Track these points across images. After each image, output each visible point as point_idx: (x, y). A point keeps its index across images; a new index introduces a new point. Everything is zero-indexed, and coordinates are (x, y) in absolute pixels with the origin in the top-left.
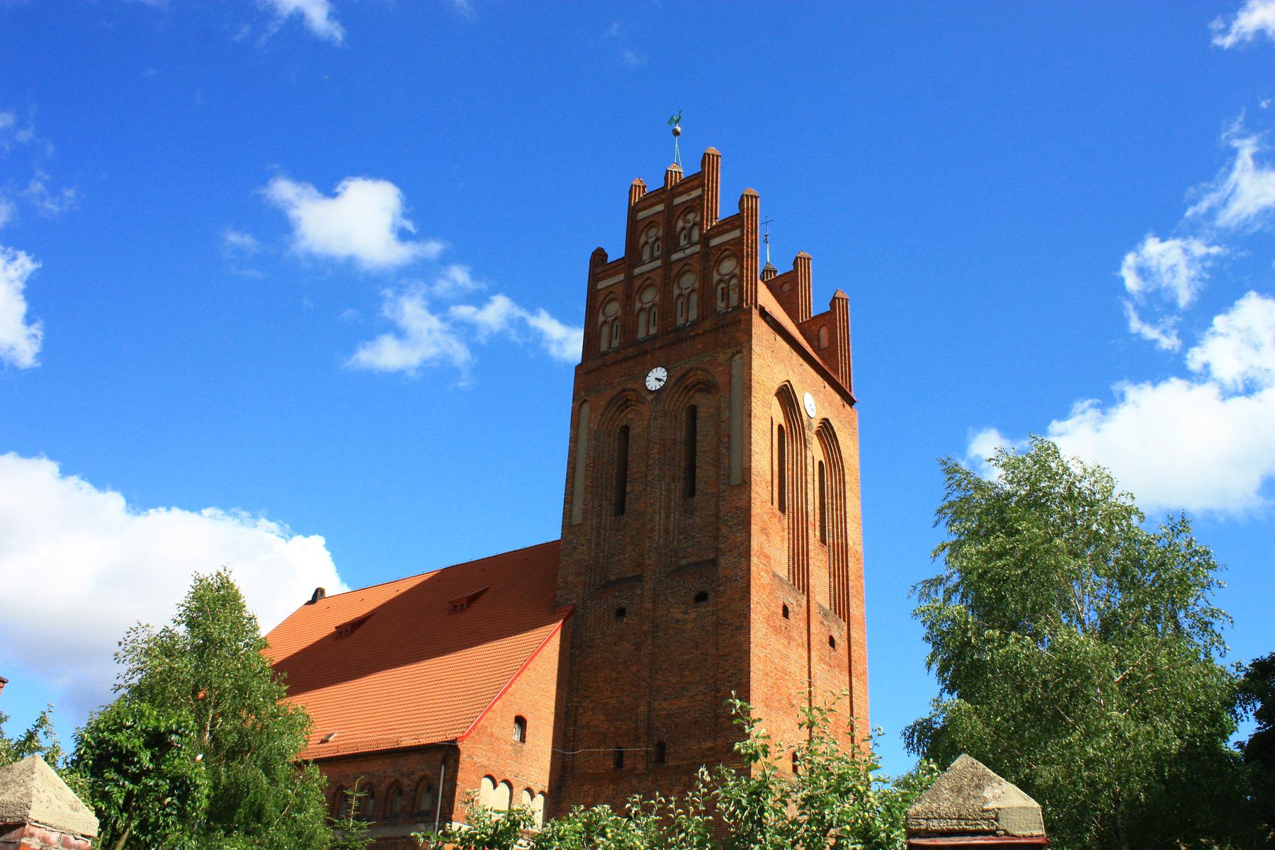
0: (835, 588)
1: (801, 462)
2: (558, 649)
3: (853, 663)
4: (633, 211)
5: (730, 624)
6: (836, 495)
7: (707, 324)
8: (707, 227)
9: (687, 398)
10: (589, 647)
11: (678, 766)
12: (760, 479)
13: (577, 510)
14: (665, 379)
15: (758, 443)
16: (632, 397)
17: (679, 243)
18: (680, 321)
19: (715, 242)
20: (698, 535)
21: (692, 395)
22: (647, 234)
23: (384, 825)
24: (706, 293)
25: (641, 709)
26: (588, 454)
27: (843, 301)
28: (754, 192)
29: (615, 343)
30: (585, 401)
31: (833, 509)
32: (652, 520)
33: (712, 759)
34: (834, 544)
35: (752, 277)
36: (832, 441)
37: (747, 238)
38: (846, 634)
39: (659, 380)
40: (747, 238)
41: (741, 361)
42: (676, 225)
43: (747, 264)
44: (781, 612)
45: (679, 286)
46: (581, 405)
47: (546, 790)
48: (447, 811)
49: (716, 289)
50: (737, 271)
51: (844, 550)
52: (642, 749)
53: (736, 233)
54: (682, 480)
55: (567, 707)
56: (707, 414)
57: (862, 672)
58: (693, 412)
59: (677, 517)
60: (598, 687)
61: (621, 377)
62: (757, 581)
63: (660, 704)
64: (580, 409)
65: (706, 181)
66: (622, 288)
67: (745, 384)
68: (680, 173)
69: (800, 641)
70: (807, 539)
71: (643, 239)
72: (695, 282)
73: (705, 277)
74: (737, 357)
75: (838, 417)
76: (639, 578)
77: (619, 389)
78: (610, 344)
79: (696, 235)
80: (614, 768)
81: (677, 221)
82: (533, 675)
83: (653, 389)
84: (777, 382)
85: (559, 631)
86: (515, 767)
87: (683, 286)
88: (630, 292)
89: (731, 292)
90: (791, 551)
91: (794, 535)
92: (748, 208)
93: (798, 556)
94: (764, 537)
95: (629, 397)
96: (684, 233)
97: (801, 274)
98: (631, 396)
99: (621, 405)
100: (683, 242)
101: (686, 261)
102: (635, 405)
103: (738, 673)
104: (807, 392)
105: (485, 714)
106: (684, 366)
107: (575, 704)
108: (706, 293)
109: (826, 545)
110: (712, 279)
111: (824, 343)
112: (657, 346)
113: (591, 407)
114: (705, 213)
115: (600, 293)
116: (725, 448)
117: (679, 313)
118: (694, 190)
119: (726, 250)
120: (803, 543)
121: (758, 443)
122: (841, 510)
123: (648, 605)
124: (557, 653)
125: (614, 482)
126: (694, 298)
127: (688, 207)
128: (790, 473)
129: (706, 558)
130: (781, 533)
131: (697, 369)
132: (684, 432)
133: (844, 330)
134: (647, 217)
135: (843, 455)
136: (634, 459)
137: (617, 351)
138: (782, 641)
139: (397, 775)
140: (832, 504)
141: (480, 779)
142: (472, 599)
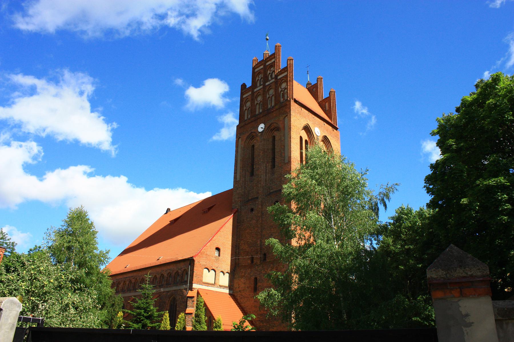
2: (232, 224)
4: (254, 69)
7: (277, 107)
8: (277, 72)
9: (272, 133)
10: (243, 222)
11: (270, 261)
12: (295, 160)
13: (238, 177)
14: (264, 127)
15: (294, 147)
16: (254, 135)
17: (268, 79)
18: (269, 106)
19: (279, 77)
20: (276, 181)
21: (273, 133)
22: (258, 77)
23: (174, 286)
24: (277, 95)
25: (258, 243)
26: (241, 156)
27: (333, 92)
28: (291, 58)
30: (240, 138)
32: (261, 177)
35: (291, 88)
36: (329, 143)
37: (289, 75)
39: (262, 128)
40: (289, 75)
43: (289, 84)
45: (269, 94)
46: (239, 139)
47: (229, 272)
49: (280, 94)
50: (286, 87)
52: (259, 256)
53: (285, 74)
54: (271, 163)
55: (236, 243)
58: (274, 138)
61: (251, 128)
64: (238, 141)
65: (276, 56)
66: (251, 97)
67: (289, 127)
68: (268, 53)
71: (257, 79)
73: (276, 90)
75: (331, 134)
76: (257, 198)
77: (250, 132)
78: (248, 117)
79: (273, 76)
80: (251, 263)
82: (222, 233)
83: (260, 131)
84: (302, 125)
85: (232, 218)
86: (216, 265)
87: (270, 94)
88: (253, 98)
92: (289, 64)
95: (253, 135)
96: (270, 75)
97: (319, 84)
98: (254, 134)
99: (251, 138)
100: (270, 78)
102: (256, 137)
104: (316, 127)
105: (203, 247)
106: (270, 122)
107: (238, 242)
108: (277, 95)
110: (279, 91)
111: (327, 108)
113: (242, 139)
114: (276, 67)
115: (244, 99)
116: (283, 150)
117: (269, 104)
119: (283, 80)
121: (294, 147)
123: (260, 207)
124: (232, 225)
125: (250, 165)
126: (273, 98)
127: (271, 66)
131: (274, 123)
132: (271, 146)
133: (334, 103)
134: (258, 71)
137: (249, 119)
141: (203, 269)
142: (210, 209)
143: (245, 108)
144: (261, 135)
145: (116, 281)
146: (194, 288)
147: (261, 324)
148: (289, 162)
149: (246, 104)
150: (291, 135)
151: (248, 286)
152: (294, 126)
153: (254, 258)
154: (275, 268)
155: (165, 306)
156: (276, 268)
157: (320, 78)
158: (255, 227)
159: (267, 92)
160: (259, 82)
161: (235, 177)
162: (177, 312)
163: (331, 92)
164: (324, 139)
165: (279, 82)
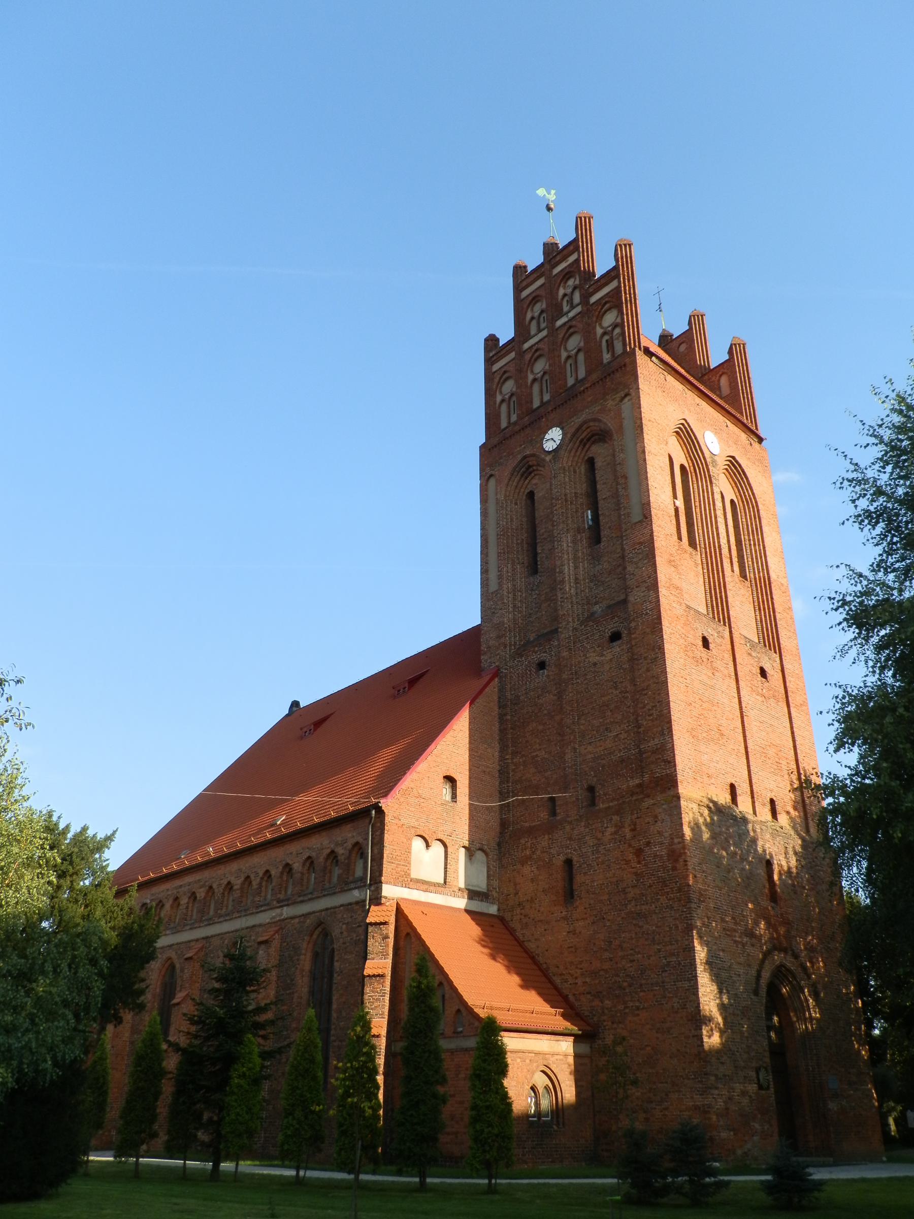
0: (761, 621)
1: (708, 498)
3: (790, 694)
5: (645, 658)
6: (753, 531)
13: (493, 575)
17: (562, 309)
20: (607, 580)
24: (590, 350)
29: (514, 418)
30: (491, 476)
31: (750, 545)
32: (561, 572)
33: (641, 796)
34: (755, 579)
36: (742, 479)
38: (779, 665)
41: (630, 402)
42: (557, 293)
43: (627, 310)
44: (701, 643)
48: (377, 874)
49: (601, 342)
50: (619, 320)
51: (767, 583)
53: (614, 284)
56: (605, 463)
57: (802, 703)
58: (591, 462)
59: (586, 566)
60: (527, 742)
61: (521, 445)
62: (669, 612)
63: (586, 749)
64: (486, 485)
69: (726, 672)
70: (723, 572)
71: (529, 316)
72: (580, 341)
73: (588, 334)
74: (626, 400)
77: (519, 457)
81: (558, 289)
88: (520, 370)
89: (615, 342)
90: (707, 586)
91: (708, 570)
93: (715, 589)
94: (673, 569)
95: (530, 463)
99: (524, 472)
101: (570, 323)
102: (537, 470)
103: (658, 704)
109: (747, 580)
112: (550, 409)
117: (569, 374)
118: (571, 255)
119: (606, 303)
120: (719, 577)
122: (759, 545)
125: (525, 546)
126: (581, 357)
128: (698, 510)
129: (617, 599)
130: (695, 569)
135: (755, 491)
136: (542, 520)
138: (705, 672)
139: (332, 846)
140: (750, 540)
143: (499, 398)
144: (554, 458)
145: (152, 900)
146: (386, 898)
147: (597, 1003)
148: (647, 518)
149: (501, 386)
150: (646, 445)
151: (547, 887)
152: (649, 420)
153: (558, 803)
154: (626, 825)
155: (298, 960)
156: (630, 825)
157: (698, 316)
158: (553, 714)
159: (561, 343)
160: (534, 324)
161: (485, 583)
162: (335, 975)
163: (735, 344)
164: (728, 465)
165: (595, 310)
